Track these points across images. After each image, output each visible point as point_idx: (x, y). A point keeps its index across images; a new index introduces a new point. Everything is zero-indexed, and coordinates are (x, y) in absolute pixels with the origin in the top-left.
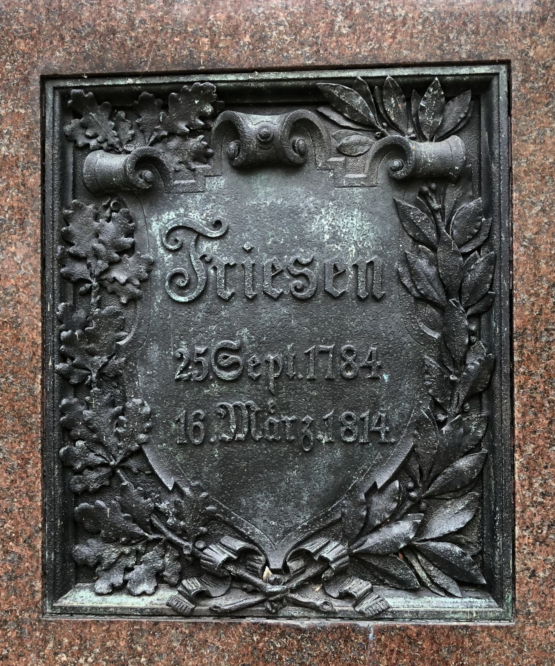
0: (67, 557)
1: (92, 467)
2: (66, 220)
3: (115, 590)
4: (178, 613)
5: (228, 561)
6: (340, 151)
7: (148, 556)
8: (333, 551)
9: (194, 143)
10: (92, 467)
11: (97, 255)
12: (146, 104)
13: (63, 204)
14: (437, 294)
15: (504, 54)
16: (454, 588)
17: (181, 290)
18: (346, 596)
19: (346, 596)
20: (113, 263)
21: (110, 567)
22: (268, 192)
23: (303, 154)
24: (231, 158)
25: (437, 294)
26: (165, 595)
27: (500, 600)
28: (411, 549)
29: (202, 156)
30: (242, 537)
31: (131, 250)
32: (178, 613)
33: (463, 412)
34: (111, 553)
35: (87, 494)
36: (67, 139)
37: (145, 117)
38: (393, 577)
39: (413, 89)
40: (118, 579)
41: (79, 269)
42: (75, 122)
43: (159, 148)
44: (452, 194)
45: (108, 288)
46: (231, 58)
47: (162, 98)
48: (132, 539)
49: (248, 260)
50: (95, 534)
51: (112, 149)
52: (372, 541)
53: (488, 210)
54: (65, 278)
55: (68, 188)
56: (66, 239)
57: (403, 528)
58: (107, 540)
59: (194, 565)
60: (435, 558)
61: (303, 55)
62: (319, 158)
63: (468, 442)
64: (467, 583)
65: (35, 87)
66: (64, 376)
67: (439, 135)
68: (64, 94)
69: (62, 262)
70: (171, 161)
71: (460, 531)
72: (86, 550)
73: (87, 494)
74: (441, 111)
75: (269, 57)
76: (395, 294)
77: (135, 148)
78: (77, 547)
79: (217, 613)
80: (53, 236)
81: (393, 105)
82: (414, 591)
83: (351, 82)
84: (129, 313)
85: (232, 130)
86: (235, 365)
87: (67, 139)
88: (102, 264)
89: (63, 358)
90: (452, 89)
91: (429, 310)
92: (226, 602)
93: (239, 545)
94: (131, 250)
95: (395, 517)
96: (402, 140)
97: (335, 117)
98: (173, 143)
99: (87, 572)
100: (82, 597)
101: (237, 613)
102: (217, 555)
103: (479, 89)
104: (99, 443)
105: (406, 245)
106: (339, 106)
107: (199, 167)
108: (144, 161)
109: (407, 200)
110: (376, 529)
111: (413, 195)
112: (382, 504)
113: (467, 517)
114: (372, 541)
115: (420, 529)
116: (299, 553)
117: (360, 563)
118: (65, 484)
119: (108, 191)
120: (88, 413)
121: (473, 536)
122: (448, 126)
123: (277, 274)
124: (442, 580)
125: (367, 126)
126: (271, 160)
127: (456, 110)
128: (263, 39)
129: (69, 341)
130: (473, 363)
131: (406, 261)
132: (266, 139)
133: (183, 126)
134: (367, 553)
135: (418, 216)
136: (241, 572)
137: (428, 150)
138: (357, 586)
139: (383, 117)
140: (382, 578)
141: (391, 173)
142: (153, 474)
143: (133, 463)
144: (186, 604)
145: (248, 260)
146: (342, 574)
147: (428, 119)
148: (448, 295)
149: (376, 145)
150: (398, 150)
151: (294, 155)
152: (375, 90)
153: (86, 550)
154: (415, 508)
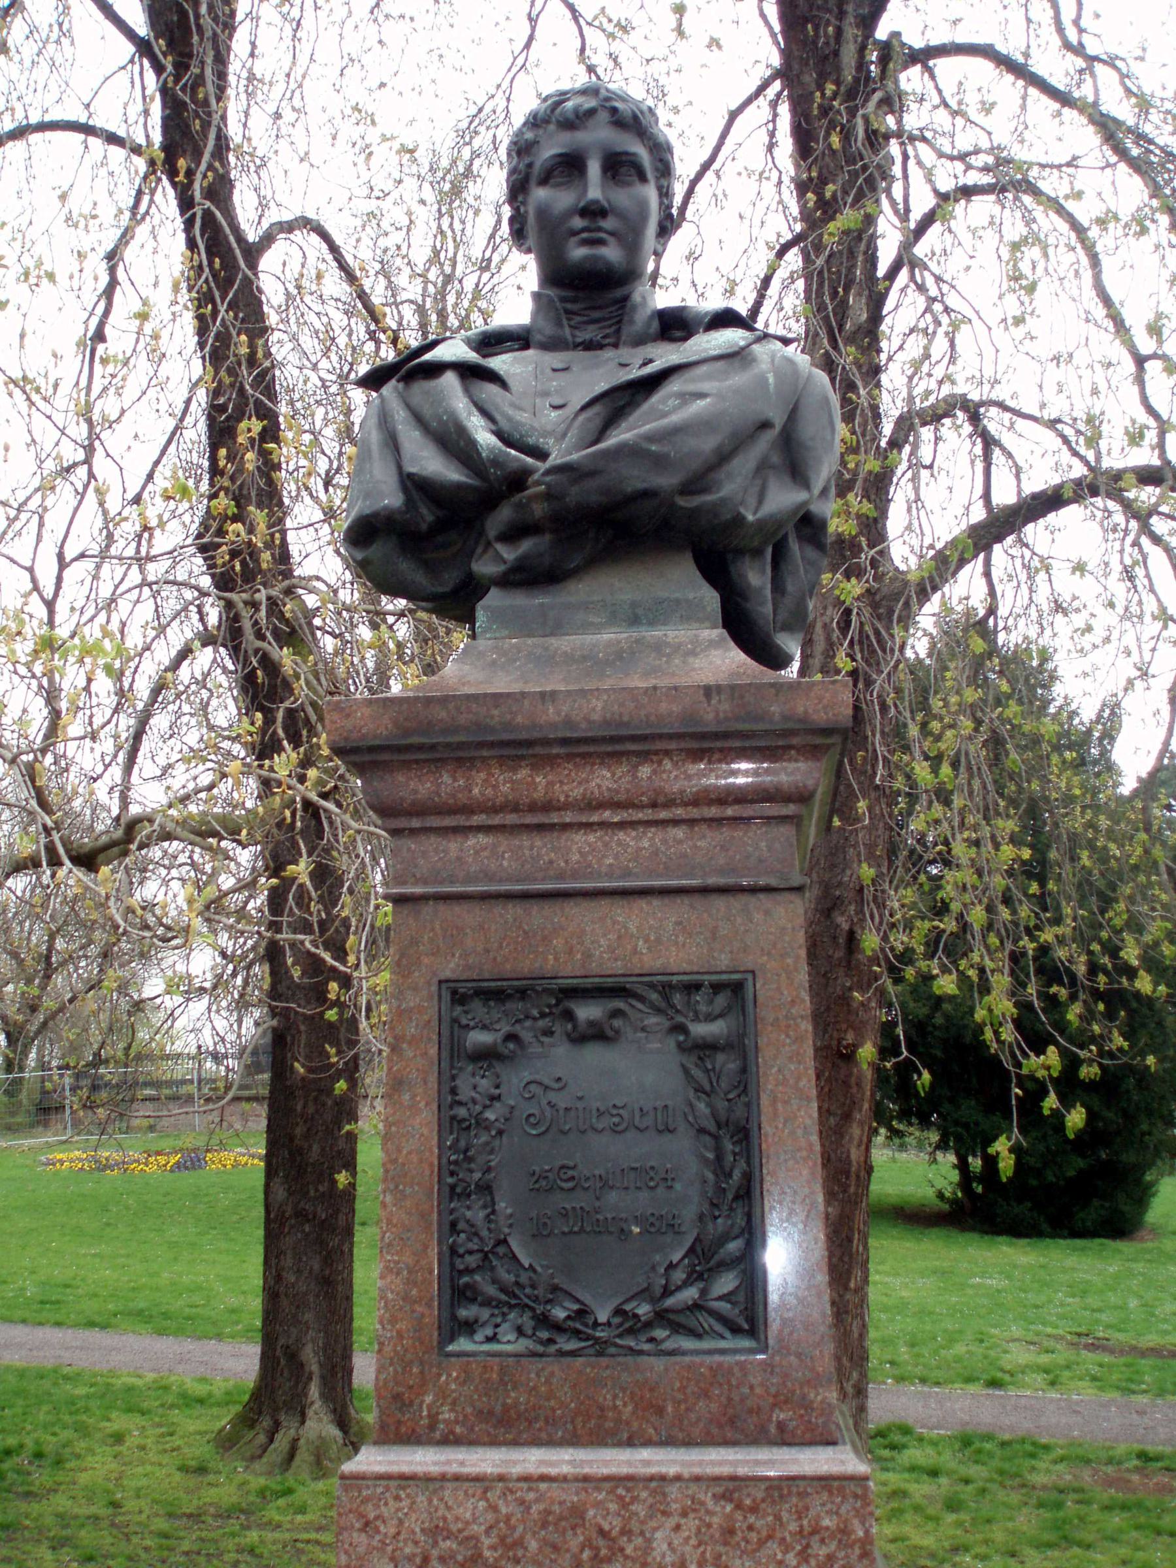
0: (454, 1317)
1: (470, 1252)
2: (453, 1078)
3: (489, 1340)
4: (534, 1354)
5: (569, 1317)
6: (643, 1029)
7: (512, 1316)
8: (644, 1310)
9: (541, 1023)
10: (470, 1252)
11: (474, 1102)
12: (510, 996)
13: (452, 1067)
14: (712, 1127)
15: (750, 967)
16: (727, 1334)
17: (534, 1126)
18: (652, 1340)
19: (652, 1340)
20: (485, 1107)
21: (483, 1325)
22: (593, 1054)
23: (617, 1032)
24: (568, 1035)
25: (712, 1127)
26: (523, 1345)
27: (757, 1340)
28: (696, 1307)
29: (549, 1033)
30: (577, 1301)
31: (498, 1098)
32: (534, 1354)
33: (731, 1209)
34: (485, 1314)
35: (468, 1271)
36: (455, 1021)
37: (509, 1005)
38: (684, 1327)
39: (692, 987)
40: (489, 1332)
41: (462, 1112)
42: (459, 1009)
43: (518, 1027)
44: (720, 1058)
45: (481, 1124)
46: (568, 971)
47: (522, 994)
48: (499, 1304)
49: (580, 1105)
50: (473, 1300)
51: (485, 1027)
52: (670, 1302)
53: (744, 1070)
54: (453, 1118)
55: (456, 1055)
56: (454, 1091)
57: (690, 1294)
58: (482, 1305)
59: (544, 1321)
60: (712, 1313)
61: (618, 967)
62: (628, 1032)
63: (736, 1231)
64: (736, 1330)
65: (434, 988)
66: (453, 1188)
67: (710, 1018)
68: (454, 992)
69: (451, 1107)
70: (526, 1036)
71: (731, 1293)
72: (463, 1313)
73: (468, 1271)
74: (711, 1002)
75: (594, 968)
76: (682, 1127)
77: (506, 1028)
78: (805, 1172)
79: (562, 1353)
80: (446, 1088)
81: (678, 999)
82: (699, 1336)
83: (652, 986)
84: (497, 1143)
85: (569, 1015)
86: (573, 1178)
87: (455, 1021)
88: (478, 1108)
89: (452, 1174)
90: (717, 988)
91: (707, 1138)
92: (573, 1345)
93: (576, 1307)
94: (498, 1098)
95: (686, 1284)
96: (596, 259)
97: (639, 1005)
98: (528, 1023)
99: (469, 1328)
100: (463, 1344)
101: (573, 1353)
102: (560, 1314)
103: (737, 988)
104: (476, 1234)
105: (691, 1094)
106: (641, 999)
107: (546, 1040)
108: (511, 1037)
109: (690, 1061)
110: (672, 1293)
111: (694, 1058)
112: (679, 1276)
113: (736, 1283)
114: (670, 1302)
115: (704, 1292)
116: (619, 1312)
117: (662, 1317)
118: (452, 1265)
119: (485, 1057)
120: (469, 1214)
121: (741, 1297)
122: (717, 1011)
123: (600, 1114)
124: (718, 1327)
125: (659, 1011)
126: (597, 1034)
127: (721, 1001)
128: (590, 956)
129: (456, 1162)
130: (737, 1175)
131: (691, 1105)
132: (591, 1024)
133: (535, 1013)
134: (667, 1311)
135: (697, 1073)
136: (578, 1326)
137: (700, 1030)
138: (660, 1333)
139: (673, 1006)
140: (678, 1328)
141: (679, 1045)
142: (514, 1257)
143: (501, 1250)
144: (540, 1349)
145: (580, 1105)
146: (648, 1325)
147: (703, 1008)
148: (719, 1127)
149: (667, 1024)
150: (680, 1029)
151: (610, 1033)
152: (666, 989)
153: (463, 1313)
154: (700, 1277)
